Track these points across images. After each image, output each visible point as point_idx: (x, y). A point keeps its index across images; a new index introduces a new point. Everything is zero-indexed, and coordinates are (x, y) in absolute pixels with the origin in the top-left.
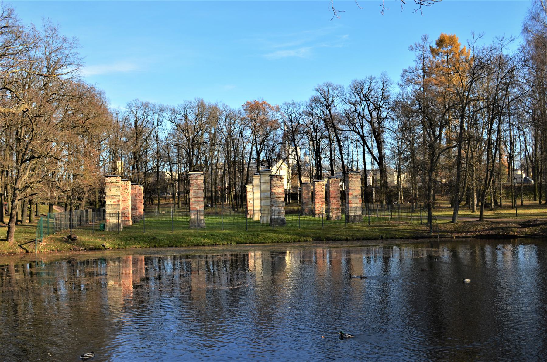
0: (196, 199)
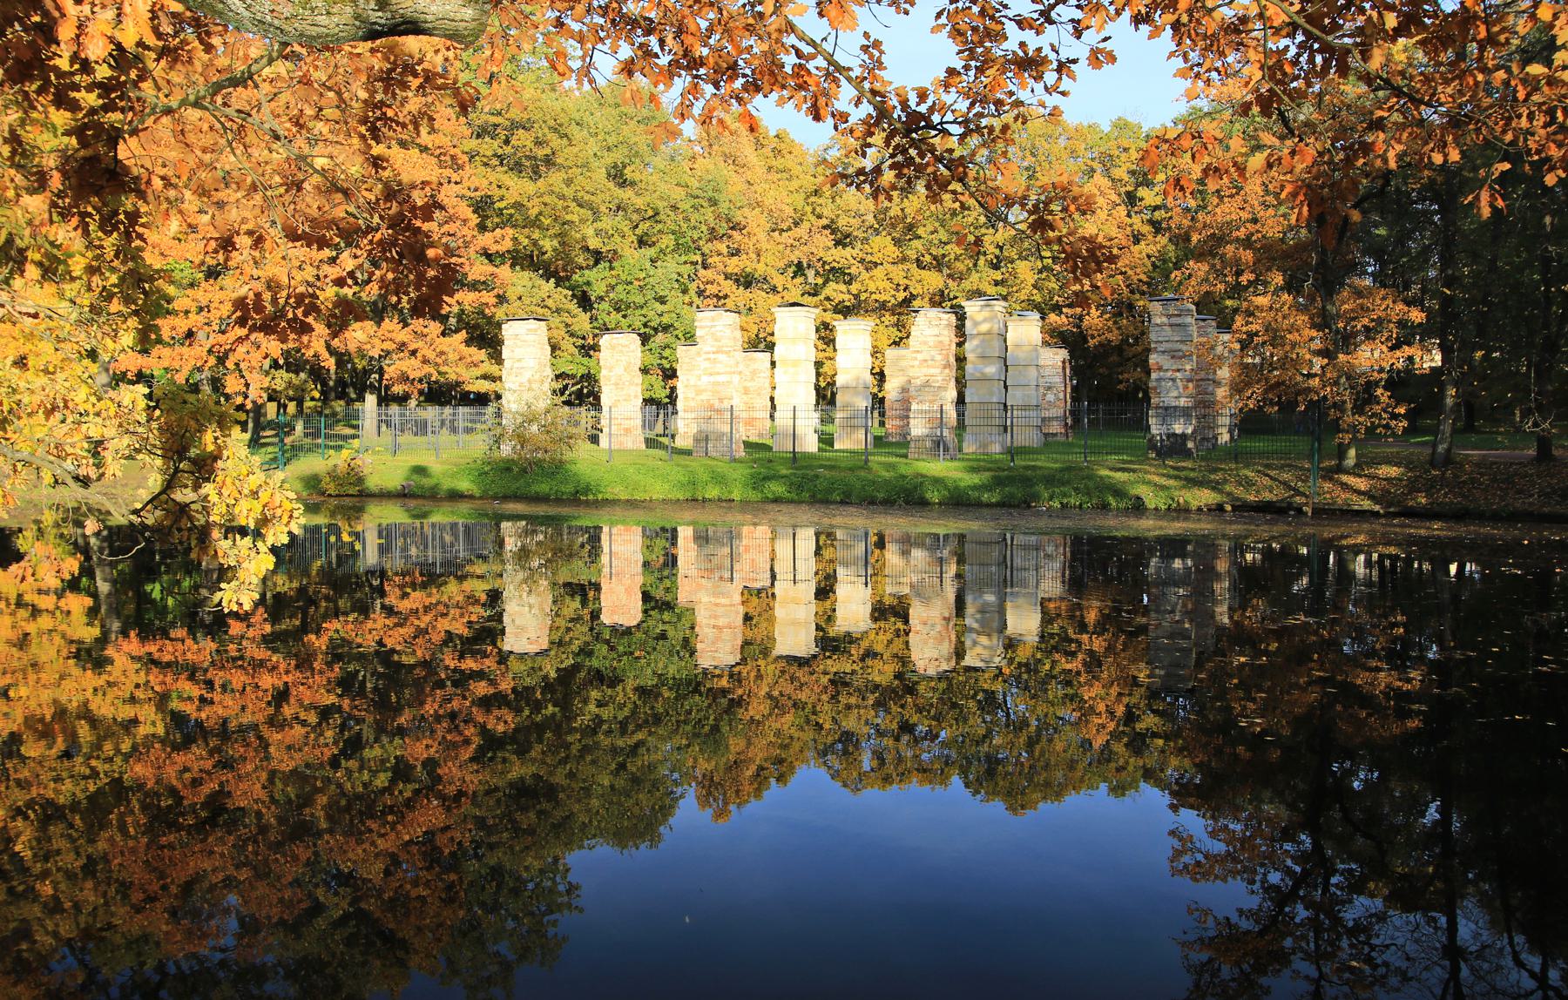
0: (712, 379)
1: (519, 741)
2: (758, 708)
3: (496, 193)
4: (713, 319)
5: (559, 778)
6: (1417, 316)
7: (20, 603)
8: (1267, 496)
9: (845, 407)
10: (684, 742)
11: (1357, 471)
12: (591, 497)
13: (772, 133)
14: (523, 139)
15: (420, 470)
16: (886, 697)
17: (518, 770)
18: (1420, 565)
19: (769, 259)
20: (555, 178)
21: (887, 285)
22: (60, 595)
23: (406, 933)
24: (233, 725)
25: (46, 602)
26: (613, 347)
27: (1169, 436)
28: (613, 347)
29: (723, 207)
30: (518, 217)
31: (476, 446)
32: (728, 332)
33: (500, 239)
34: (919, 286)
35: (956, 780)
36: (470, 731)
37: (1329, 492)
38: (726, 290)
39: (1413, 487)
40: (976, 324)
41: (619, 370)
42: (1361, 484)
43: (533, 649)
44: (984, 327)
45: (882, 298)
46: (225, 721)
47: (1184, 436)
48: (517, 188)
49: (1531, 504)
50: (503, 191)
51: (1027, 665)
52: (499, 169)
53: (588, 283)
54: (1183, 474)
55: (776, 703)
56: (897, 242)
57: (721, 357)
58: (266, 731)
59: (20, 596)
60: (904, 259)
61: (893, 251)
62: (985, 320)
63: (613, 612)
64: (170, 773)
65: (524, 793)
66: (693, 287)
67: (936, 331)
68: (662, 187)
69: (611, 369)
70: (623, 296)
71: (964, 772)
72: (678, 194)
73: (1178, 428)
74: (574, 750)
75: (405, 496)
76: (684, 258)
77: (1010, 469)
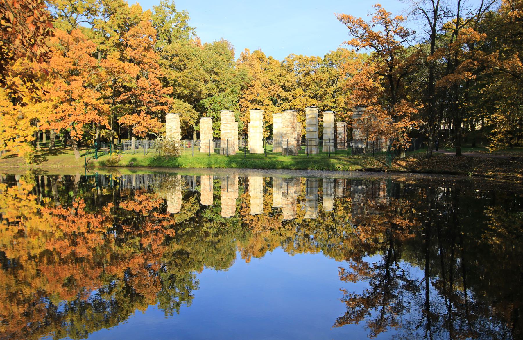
0: (225, 132)
1: (178, 238)
2: (257, 230)
3: (167, 76)
4: (226, 114)
5: (189, 250)
6: (415, 111)
7: (16, 198)
8: (370, 167)
9: (275, 140)
10: (235, 240)
11: (404, 159)
12: (183, 167)
13: (267, 57)
14: (176, 60)
15: (134, 160)
16: (300, 226)
17: (176, 247)
18: (448, 189)
19: (263, 94)
20: (186, 72)
21: (300, 103)
22: (28, 195)
23: (143, 293)
24: (77, 233)
25: (24, 197)
26: (203, 122)
27: (356, 148)
28: (203, 122)
29: (246, 80)
30: (176, 84)
31: (153, 153)
32: (230, 117)
33: (170, 89)
34: (310, 104)
35: (321, 252)
36: (161, 235)
37: (395, 167)
38: (248, 105)
39: (419, 164)
40: (308, 115)
41: (205, 129)
42: (403, 164)
43: (175, 212)
44: (310, 116)
45: (299, 107)
46: (74, 232)
47: (362, 149)
48: (173, 75)
49: (450, 169)
50: (170, 76)
51: (342, 217)
52: (169, 69)
53: (204, 103)
54: (351, 160)
55: (264, 228)
56: (304, 90)
57: (228, 125)
58: (86, 235)
59: (16, 195)
60: (305, 95)
61: (302, 93)
62: (310, 114)
63: (204, 201)
64: (57, 246)
65: (181, 253)
66: (238, 104)
67: (290, 117)
68: (226, 74)
69: (203, 129)
70: (215, 107)
71: (323, 249)
72: (231, 76)
73: (360, 146)
74: (193, 242)
75: (131, 166)
76: (235, 95)
77: (307, 158)
